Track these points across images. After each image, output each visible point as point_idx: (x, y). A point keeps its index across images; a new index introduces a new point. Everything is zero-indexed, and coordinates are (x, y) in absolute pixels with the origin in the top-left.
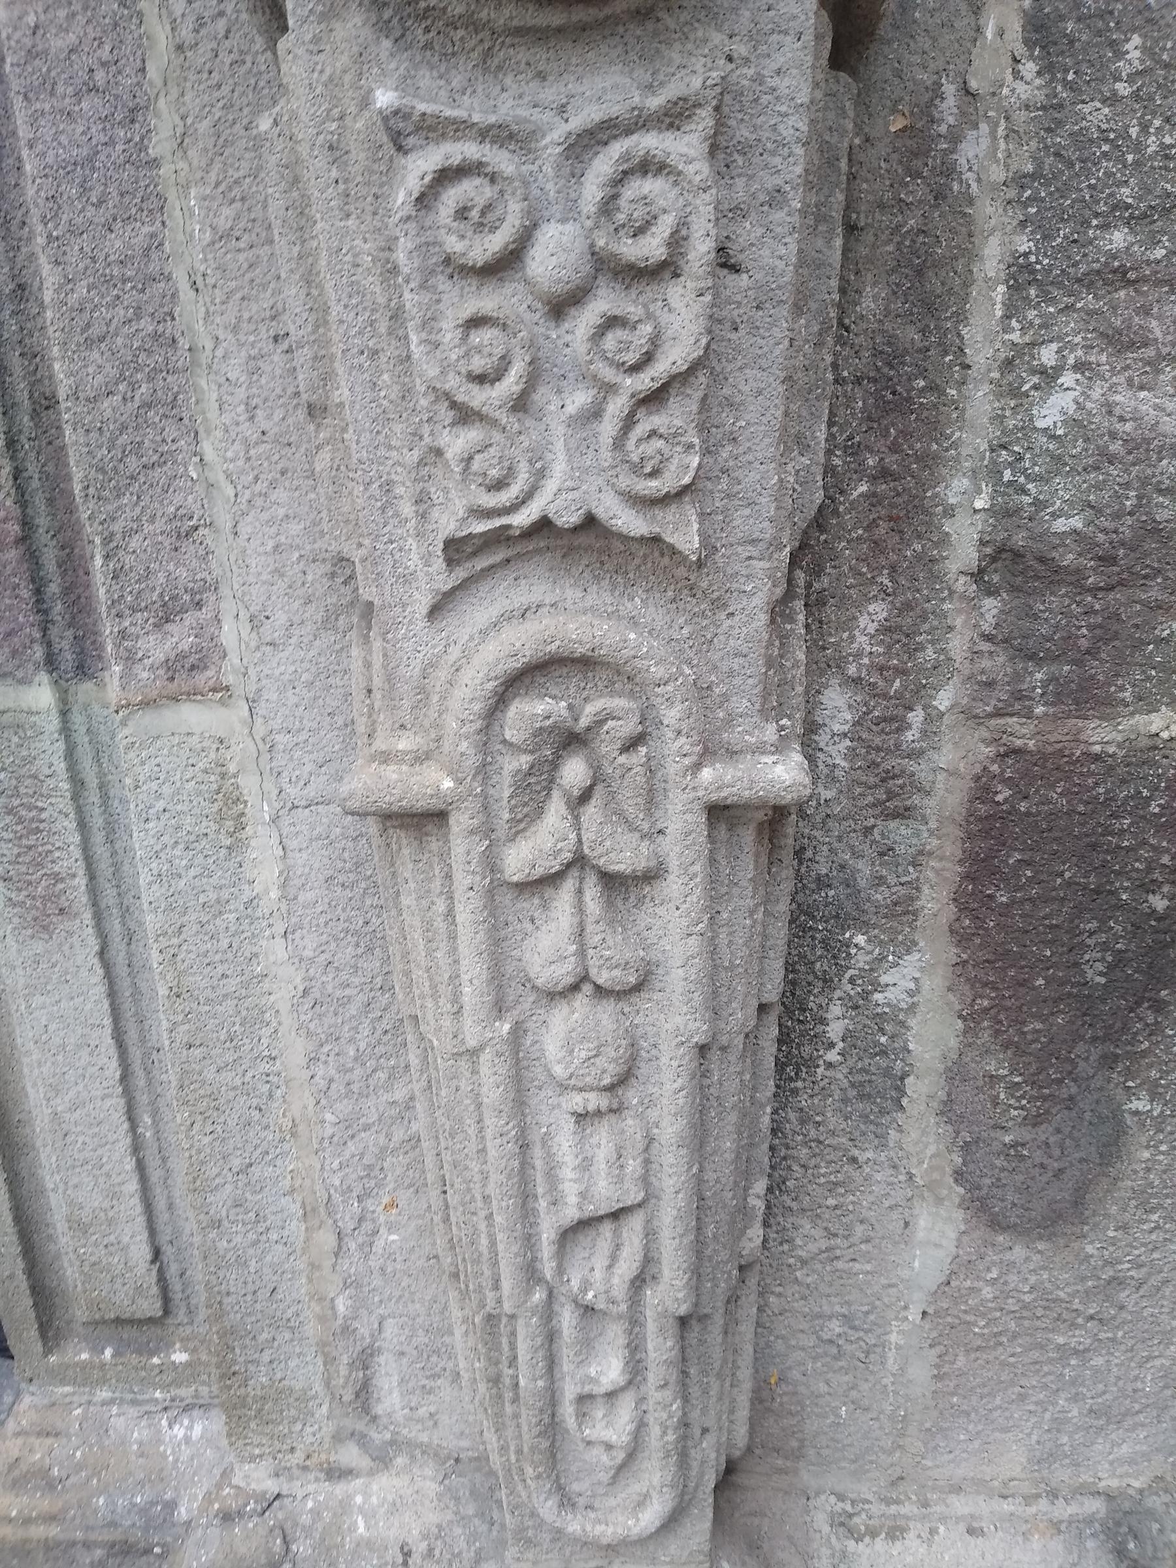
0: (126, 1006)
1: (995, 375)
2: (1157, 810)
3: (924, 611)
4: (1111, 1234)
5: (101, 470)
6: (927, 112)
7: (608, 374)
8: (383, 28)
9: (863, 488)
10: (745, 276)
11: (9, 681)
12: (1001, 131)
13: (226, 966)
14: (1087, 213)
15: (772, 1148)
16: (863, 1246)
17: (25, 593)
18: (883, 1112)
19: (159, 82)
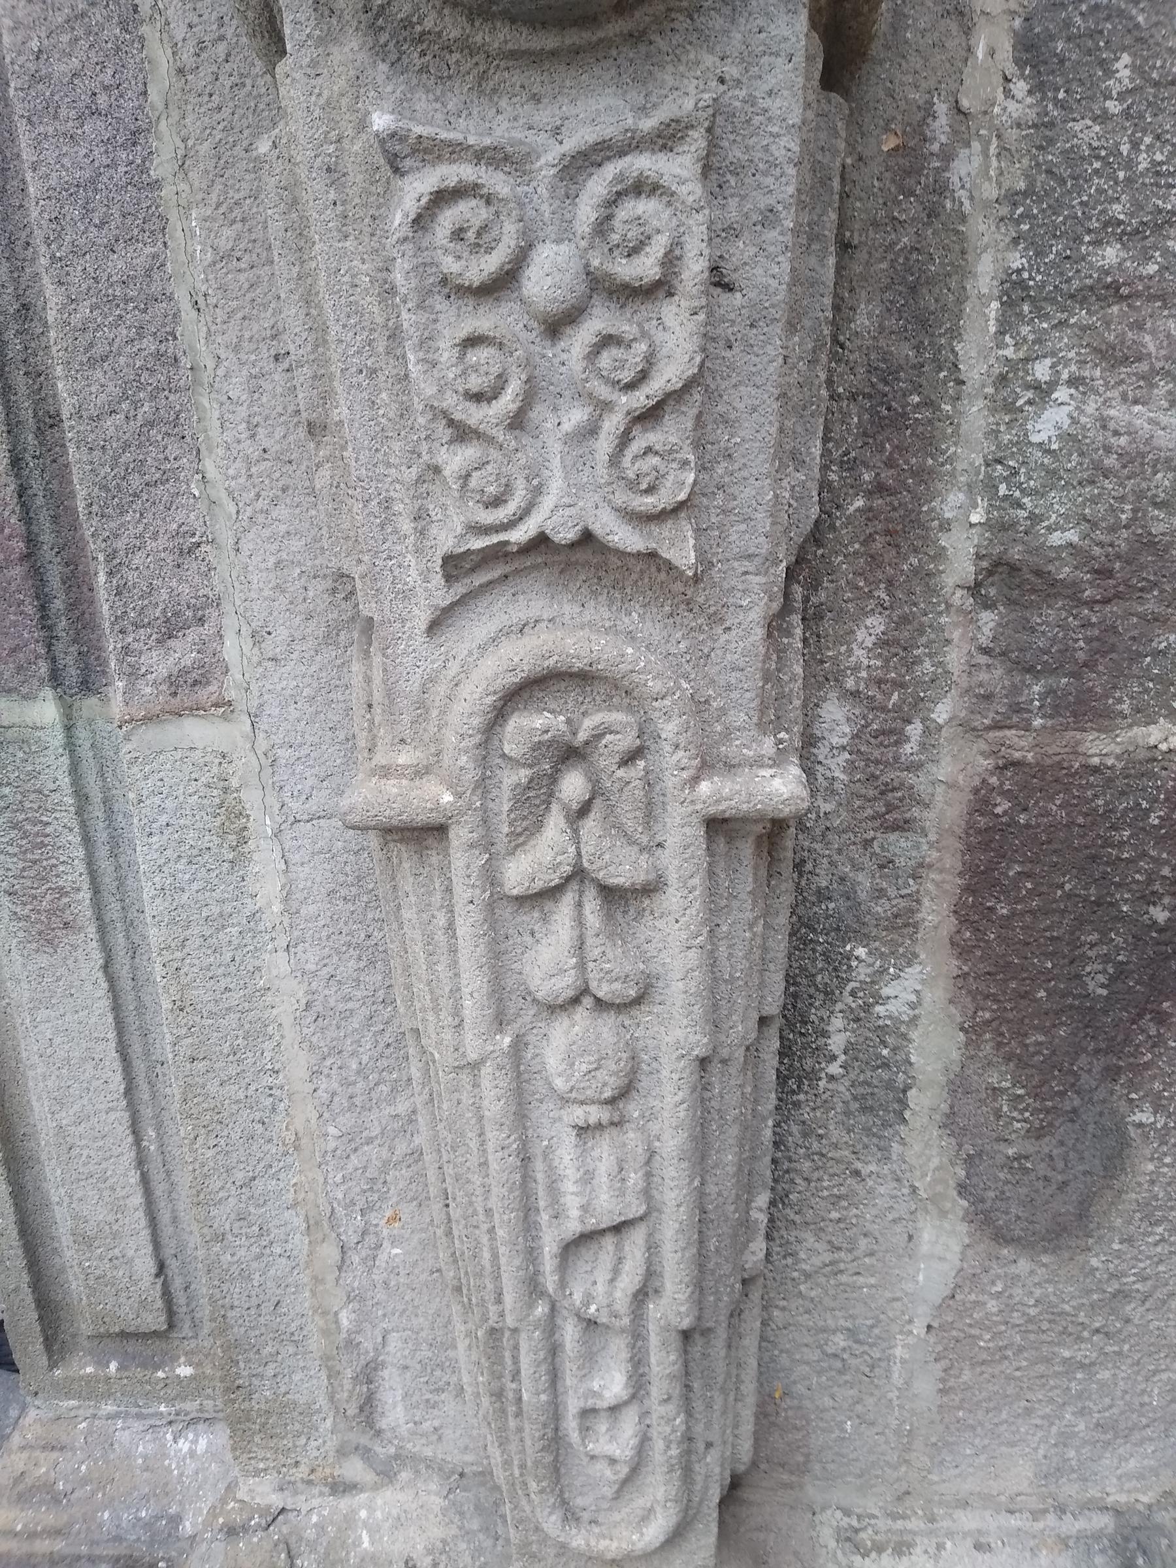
0: (130, 1019)
1: (990, 390)
2: (1156, 822)
3: (922, 625)
4: (1116, 1246)
5: (105, 488)
6: (919, 131)
7: (604, 392)
8: (379, 51)
9: (859, 503)
10: (738, 295)
11: (15, 696)
12: (993, 149)
13: (229, 979)
14: (1080, 229)
15: (774, 1161)
16: (867, 1260)
17: (29, 610)
18: (886, 1125)
19: (160, 106)
